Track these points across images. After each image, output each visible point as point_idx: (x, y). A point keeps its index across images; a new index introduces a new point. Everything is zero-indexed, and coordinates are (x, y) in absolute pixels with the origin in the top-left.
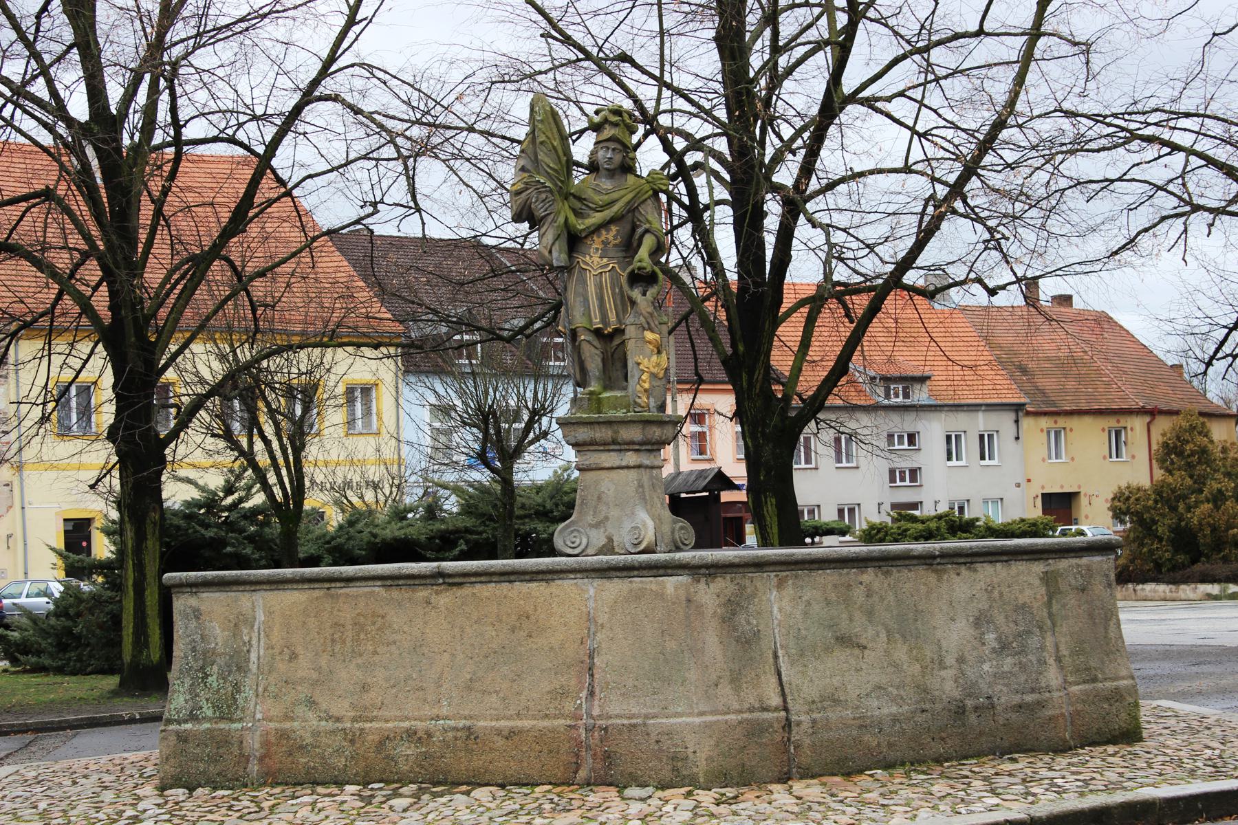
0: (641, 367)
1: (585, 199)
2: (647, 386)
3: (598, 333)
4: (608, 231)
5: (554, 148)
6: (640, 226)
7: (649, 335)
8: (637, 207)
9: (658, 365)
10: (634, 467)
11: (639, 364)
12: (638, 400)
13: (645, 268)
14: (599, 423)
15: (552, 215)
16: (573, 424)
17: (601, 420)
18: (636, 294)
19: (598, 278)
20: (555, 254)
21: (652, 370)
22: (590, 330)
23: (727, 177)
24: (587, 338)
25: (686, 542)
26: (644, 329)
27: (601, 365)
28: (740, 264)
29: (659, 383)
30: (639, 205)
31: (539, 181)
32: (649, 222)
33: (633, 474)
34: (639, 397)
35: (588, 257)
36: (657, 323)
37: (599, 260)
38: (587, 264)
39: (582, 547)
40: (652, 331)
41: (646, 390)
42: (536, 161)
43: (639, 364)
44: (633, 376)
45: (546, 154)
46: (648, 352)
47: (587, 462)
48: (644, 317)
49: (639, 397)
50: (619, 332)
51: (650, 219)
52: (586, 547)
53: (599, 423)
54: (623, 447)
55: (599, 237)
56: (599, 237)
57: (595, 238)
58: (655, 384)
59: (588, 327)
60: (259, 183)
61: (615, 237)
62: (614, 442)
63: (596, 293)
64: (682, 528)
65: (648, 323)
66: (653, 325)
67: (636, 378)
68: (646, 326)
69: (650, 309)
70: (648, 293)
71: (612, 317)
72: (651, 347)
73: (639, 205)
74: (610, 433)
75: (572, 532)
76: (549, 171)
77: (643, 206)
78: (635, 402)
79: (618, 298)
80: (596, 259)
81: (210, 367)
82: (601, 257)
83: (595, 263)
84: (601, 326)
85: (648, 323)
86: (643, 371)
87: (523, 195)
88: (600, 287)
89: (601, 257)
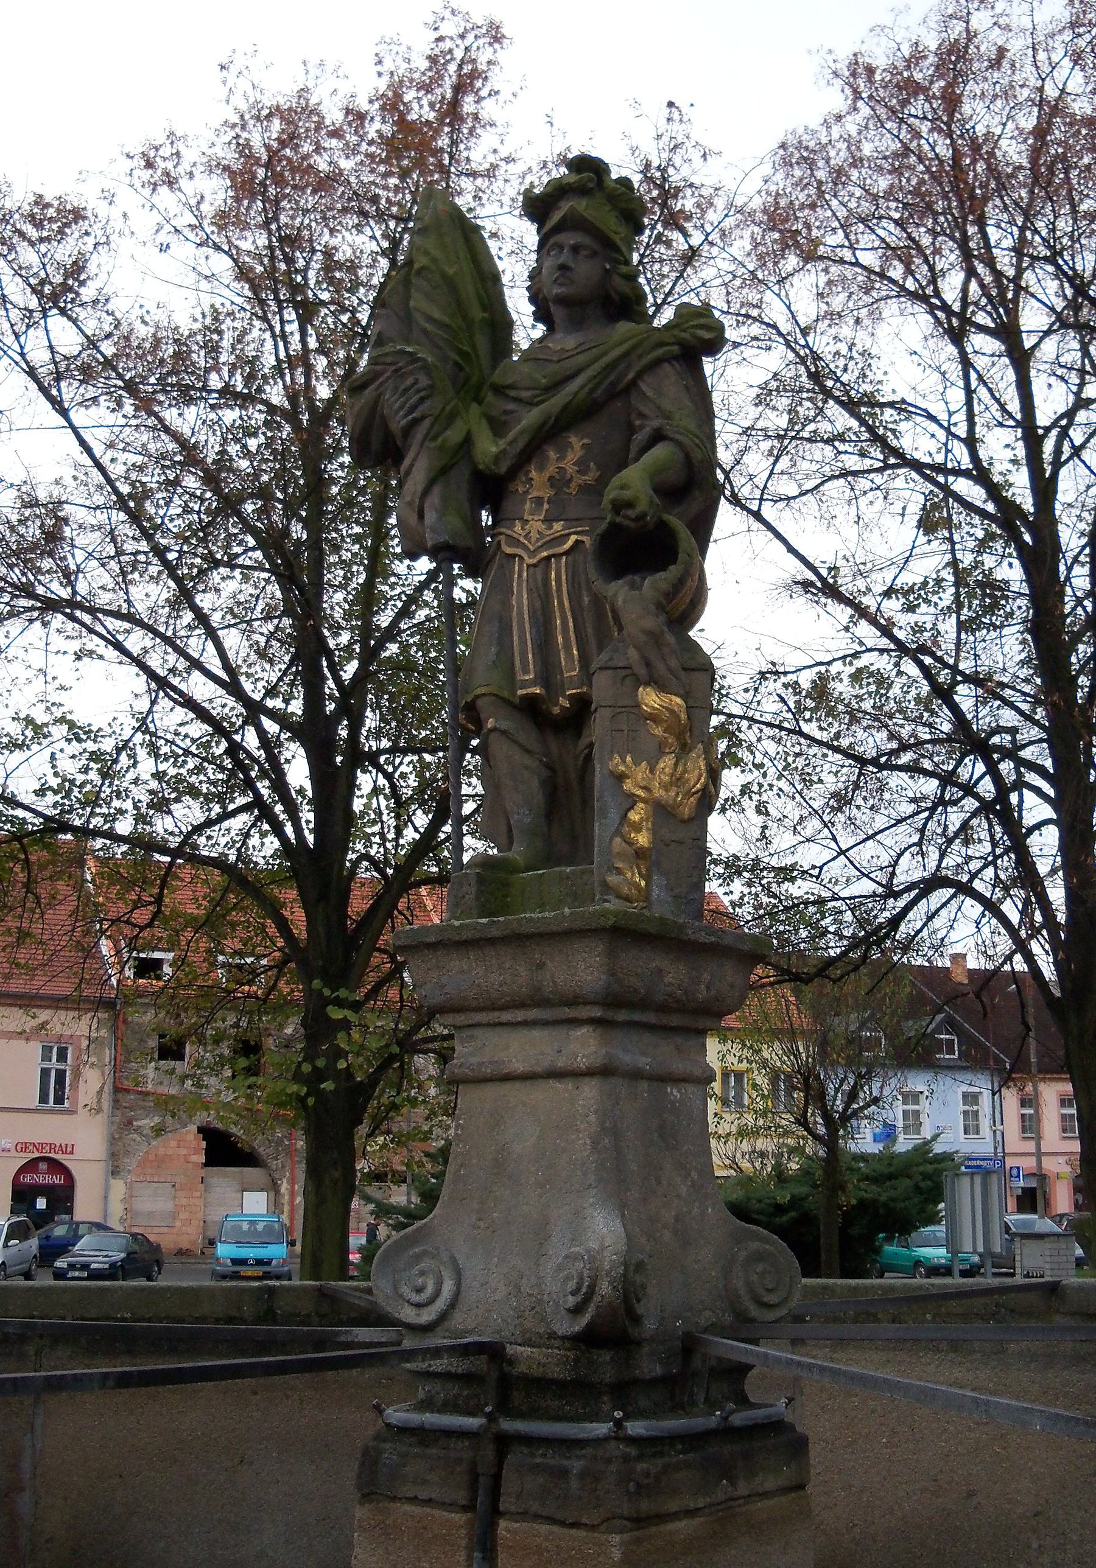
0: (628, 786)
1: (512, 387)
2: (643, 839)
3: (531, 708)
6: (642, 427)
7: (651, 699)
8: (633, 383)
9: (677, 781)
10: (589, 1073)
11: (621, 778)
12: (612, 879)
13: (630, 505)
14: (492, 941)
15: (427, 423)
16: (429, 946)
17: (495, 933)
18: (619, 591)
19: (539, 572)
20: (430, 517)
21: (659, 793)
23: (1051, 792)
24: (504, 725)
25: (772, 1299)
26: (639, 682)
27: (539, 798)
30: (639, 375)
31: (402, 352)
33: (590, 1092)
34: (619, 872)
35: (518, 528)
36: (674, 663)
38: (516, 543)
39: (440, 1304)
40: (662, 687)
41: (640, 854)
42: (407, 317)
43: (621, 778)
44: (604, 813)
47: (474, 1060)
48: (639, 649)
49: (619, 872)
50: (582, 707)
52: (453, 1305)
53: (492, 941)
54: (675, 1020)
55: (541, 468)
56: (541, 468)
57: (533, 474)
59: (506, 694)
61: (582, 466)
62: (537, 1000)
64: (759, 1257)
65: (648, 664)
66: (660, 668)
67: (614, 816)
68: (642, 671)
69: (651, 623)
71: (570, 669)
72: (658, 731)
73: (639, 375)
74: (523, 971)
75: (418, 1258)
76: (428, 327)
77: (647, 378)
78: (605, 884)
79: (589, 618)
80: (536, 525)
82: (548, 520)
83: (534, 535)
85: (648, 664)
86: (632, 801)
87: (369, 392)
88: (542, 595)
89: (548, 520)
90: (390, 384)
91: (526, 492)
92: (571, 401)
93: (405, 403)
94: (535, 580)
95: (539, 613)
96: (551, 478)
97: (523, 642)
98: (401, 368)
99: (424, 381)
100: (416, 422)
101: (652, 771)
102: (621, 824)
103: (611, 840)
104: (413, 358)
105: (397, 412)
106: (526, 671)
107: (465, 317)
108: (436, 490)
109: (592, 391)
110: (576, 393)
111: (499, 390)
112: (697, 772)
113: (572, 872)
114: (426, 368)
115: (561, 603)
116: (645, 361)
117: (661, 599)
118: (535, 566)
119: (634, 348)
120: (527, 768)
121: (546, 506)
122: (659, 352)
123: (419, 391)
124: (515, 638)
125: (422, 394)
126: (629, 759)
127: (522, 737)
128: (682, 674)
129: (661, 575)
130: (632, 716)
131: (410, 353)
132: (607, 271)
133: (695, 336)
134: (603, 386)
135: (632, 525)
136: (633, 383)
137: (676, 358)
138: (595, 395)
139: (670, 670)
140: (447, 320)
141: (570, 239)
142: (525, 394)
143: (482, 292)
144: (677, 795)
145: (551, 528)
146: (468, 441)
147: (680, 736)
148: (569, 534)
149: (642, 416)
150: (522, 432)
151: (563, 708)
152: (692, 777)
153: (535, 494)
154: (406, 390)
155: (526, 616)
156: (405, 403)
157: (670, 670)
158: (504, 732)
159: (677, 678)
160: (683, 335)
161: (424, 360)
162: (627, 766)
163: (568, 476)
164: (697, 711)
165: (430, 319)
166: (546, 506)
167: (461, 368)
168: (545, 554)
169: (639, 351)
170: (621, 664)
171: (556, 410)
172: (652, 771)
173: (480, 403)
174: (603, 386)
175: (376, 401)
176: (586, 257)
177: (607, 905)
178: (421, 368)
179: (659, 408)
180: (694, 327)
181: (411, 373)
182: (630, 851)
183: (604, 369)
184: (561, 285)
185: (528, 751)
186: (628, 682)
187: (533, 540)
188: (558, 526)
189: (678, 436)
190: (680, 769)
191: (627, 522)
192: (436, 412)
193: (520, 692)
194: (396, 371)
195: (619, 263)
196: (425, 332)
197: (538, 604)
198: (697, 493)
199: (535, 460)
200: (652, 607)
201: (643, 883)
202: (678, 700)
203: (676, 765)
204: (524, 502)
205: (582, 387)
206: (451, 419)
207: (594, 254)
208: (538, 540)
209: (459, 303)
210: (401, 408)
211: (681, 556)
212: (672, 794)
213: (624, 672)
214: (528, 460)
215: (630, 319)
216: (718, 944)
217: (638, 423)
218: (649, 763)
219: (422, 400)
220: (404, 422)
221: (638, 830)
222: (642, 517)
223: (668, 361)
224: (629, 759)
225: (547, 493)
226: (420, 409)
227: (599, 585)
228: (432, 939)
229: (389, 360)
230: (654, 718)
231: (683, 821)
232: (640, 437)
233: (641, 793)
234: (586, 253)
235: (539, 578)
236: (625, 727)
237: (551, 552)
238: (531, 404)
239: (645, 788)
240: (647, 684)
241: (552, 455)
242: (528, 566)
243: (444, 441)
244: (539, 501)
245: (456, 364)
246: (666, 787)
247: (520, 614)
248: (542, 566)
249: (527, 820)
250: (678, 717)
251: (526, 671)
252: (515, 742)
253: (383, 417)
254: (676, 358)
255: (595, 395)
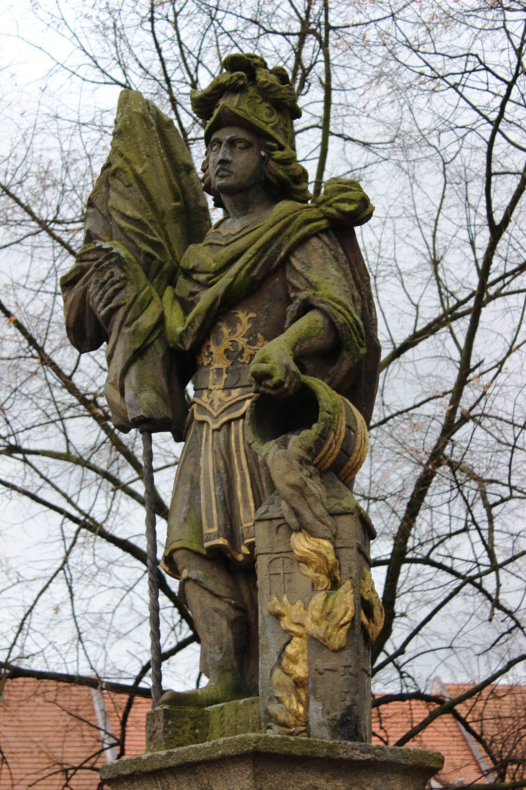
0: (285, 623)
4: (233, 324)
5: (138, 179)
6: (296, 298)
9: (328, 615)
12: (274, 708)
13: (268, 376)
15: (122, 311)
17: (172, 762)
19: (221, 435)
20: (129, 393)
21: (311, 627)
22: (197, 554)
26: (291, 530)
28: (153, 249)
29: (334, 662)
30: (290, 252)
31: (100, 249)
32: (311, 285)
34: (279, 700)
36: (319, 510)
37: (221, 394)
41: (299, 683)
43: (278, 616)
45: (121, 193)
46: (305, 586)
49: (279, 700)
51: (313, 277)
55: (218, 343)
56: (218, 343)
57: (213, 349)
58: (320, 664)
59: (195, 547)
60: (407, 512)
63: (217, 471)
65: (297, 514)
66: (308, 517)
68: (292, 520)
70: (290, 444)
72: (310, 572)
73: (290, 252)
76: (123, 224)
77: (299, 254)
80: (219, 394)
81: (81, 767)
82: (227, 388)
83: (216, 403)
84: (221, 541)
85: (297, 514)
86: (290, 636)
89: (227, 388)
90: (93, 279)
91: (209, 364)
92: (232, 283)
93: (103, 295)
94: (219, 444)
95: (223, 471)
96: (226, 351)
97: (209, 500)
98: (101, 263)
99: (118, 273)
100: (113, 311)
101: (306, 608)
102: (280, 658)
103: (272, 671)
104: (109, 253)
105: (98, 304)
106: (210, 526)
107: (154, 207)
108: (133, 371)
109: (249, 271)
110: (236, 275)
111: (188, 273)
112: (343, 607)
113: (245, 704)
114: (120, 262)
115: (240, 461)
116: (294, 239)
117: (303, 454)
118: (218, 430)
119: (286, 226)
120: (216, 611)
121: (225, 376)
122: (306, 229)
123: (113, 284)
124: (202, 496)
125: (117, 286)
126: (285, 599)
127: (210, 584)
128: (329, 520)
129: (305, 433)
130: (287, 560)
131: (107, 250)
132: (263, 158)
133: (338, 210)
134: (259, 266)
135: (272, 392)
136: (286, 260)
137: (325, 231)
138: (253, 275)
139: (316, 517)
140: (138, 216)
141: (225, 135)
142: (202, 277)
143: (174, 182)
144: (327, 628)
145: (229, 395)
146: (161, 321)
147: (330, 575)
148: (244, 400)
149: (296, 289)
150: (197, 315)
151: (245, 555)
152: (339, 611)
153: (216, 366)
154: (104, 283)
155: (211, 476)
156: (103, 295)
157: (316, 517)
158: (196, 581)
159: (323, 523)
160: (330, 210)
161: (118, 254)
162: (284, 606)
163: (240, 349)
164: (344, 551)
165: (124, 216)
166: (225, 376)
167: (153, 258)
168: (225, 419)
169: (289, 230)
170: (276, 515)
171: (221, 291)
172: (306, 608)
173: (174, 286)
174: (259, 266)
175: (85, 292)
176: (242, 149)
177: (269, 731)
178: (116, 262)
179: (307, 280)
180: (339, 201)
181: (108, 267)
182: (289, 681)
183: (258, 250)
184: (222, 177)
185: (218, 597)
186: (282, 530)
187: (216, 407)
188: (235, 393)
189: (322, 305)
190: (330, 604)
191: (268, 391)
192: (129, 301)
193: (206, 545)
194: (97, 266)
195: (273, 149)
196: (122, 229)
197: (221, 464)
198: (345, 353)
199: (212, 337)
200: (296, 463)
201: (301, 709)
202: (326, 543)
203: (326, 600)
204: (208, 373)
205: (241, 269)
206: (144, 306)
207: (248, 146)
208: (219, 406)
209: (149, 197)
210: (100, 300)
211: (322, 415)
212: (323, 627)
213: (277, 523)
214: (208, 337)
215: (291, 198)
216: (376, 761)
217: (292, 295)
218: (303, 600)
219: (117, 292)
220: (103, 313)
221: (295, 662)
222: (281, 383)
223: (316, 235)
224: (285, 599)
225: (223, 364)
226: (116, 299)
227: (256, 446)
228: (127, 771)
229: (91, 256)
230: (304, 561)
231: (334, 651)
232: (293, 308)
233: (295, 629)
234: (241, 145)
235: (222, 439)
236: (281, 571)
237: (230, 416)
238: (206, 285)
239: (298, 624)
240: (298, 531)
241: (225, 330)
242: (214, 431)
243: (138, 325)
244: (219, 371)
245: (148, 254)
246: (317, 622)
247: (206, 474)
248: (224, 429)
249: (219, 657)
250: (325, 558)
251: (210, 526)
252: (206, 589)
253: (90, 307)
254: (325, 231)
255: (253, 275)
